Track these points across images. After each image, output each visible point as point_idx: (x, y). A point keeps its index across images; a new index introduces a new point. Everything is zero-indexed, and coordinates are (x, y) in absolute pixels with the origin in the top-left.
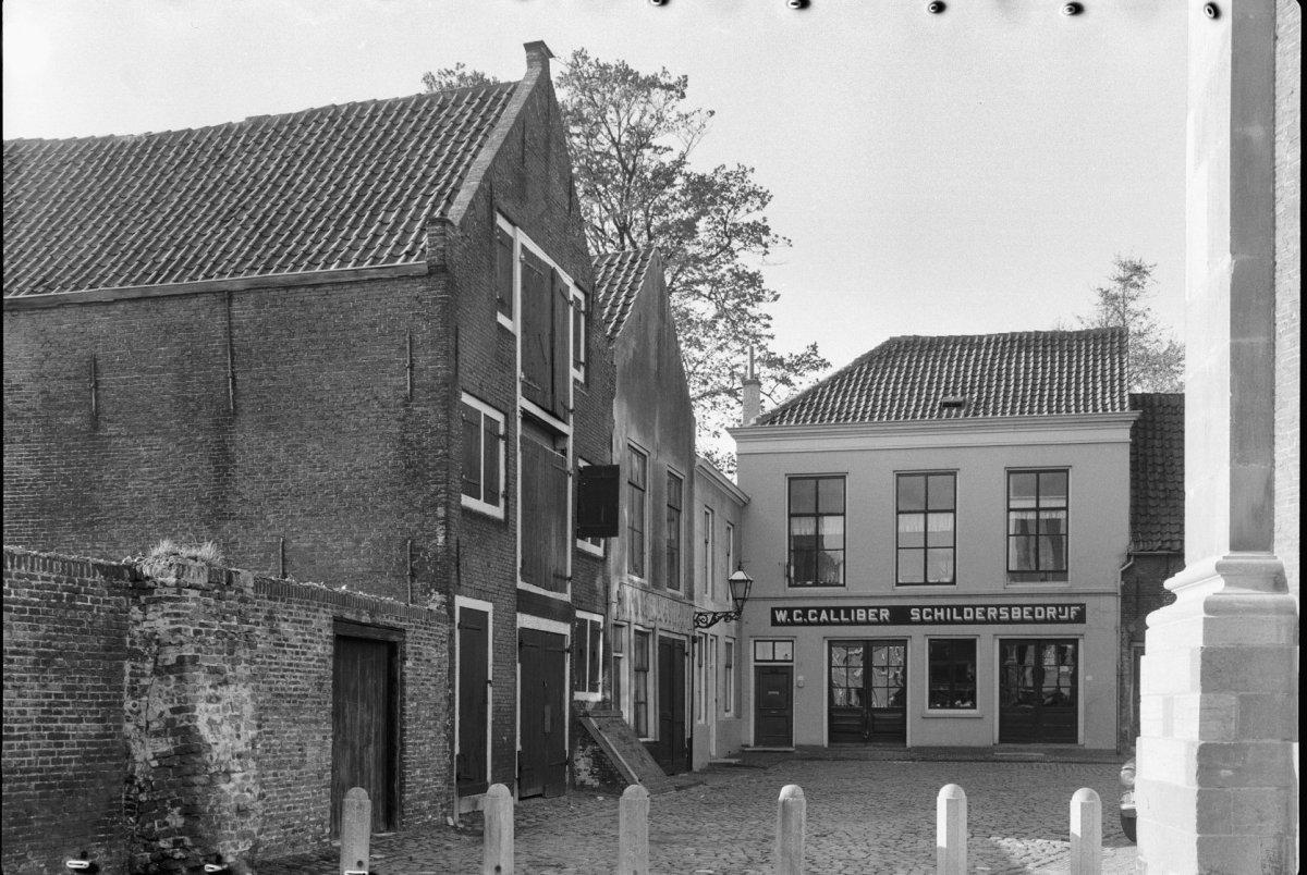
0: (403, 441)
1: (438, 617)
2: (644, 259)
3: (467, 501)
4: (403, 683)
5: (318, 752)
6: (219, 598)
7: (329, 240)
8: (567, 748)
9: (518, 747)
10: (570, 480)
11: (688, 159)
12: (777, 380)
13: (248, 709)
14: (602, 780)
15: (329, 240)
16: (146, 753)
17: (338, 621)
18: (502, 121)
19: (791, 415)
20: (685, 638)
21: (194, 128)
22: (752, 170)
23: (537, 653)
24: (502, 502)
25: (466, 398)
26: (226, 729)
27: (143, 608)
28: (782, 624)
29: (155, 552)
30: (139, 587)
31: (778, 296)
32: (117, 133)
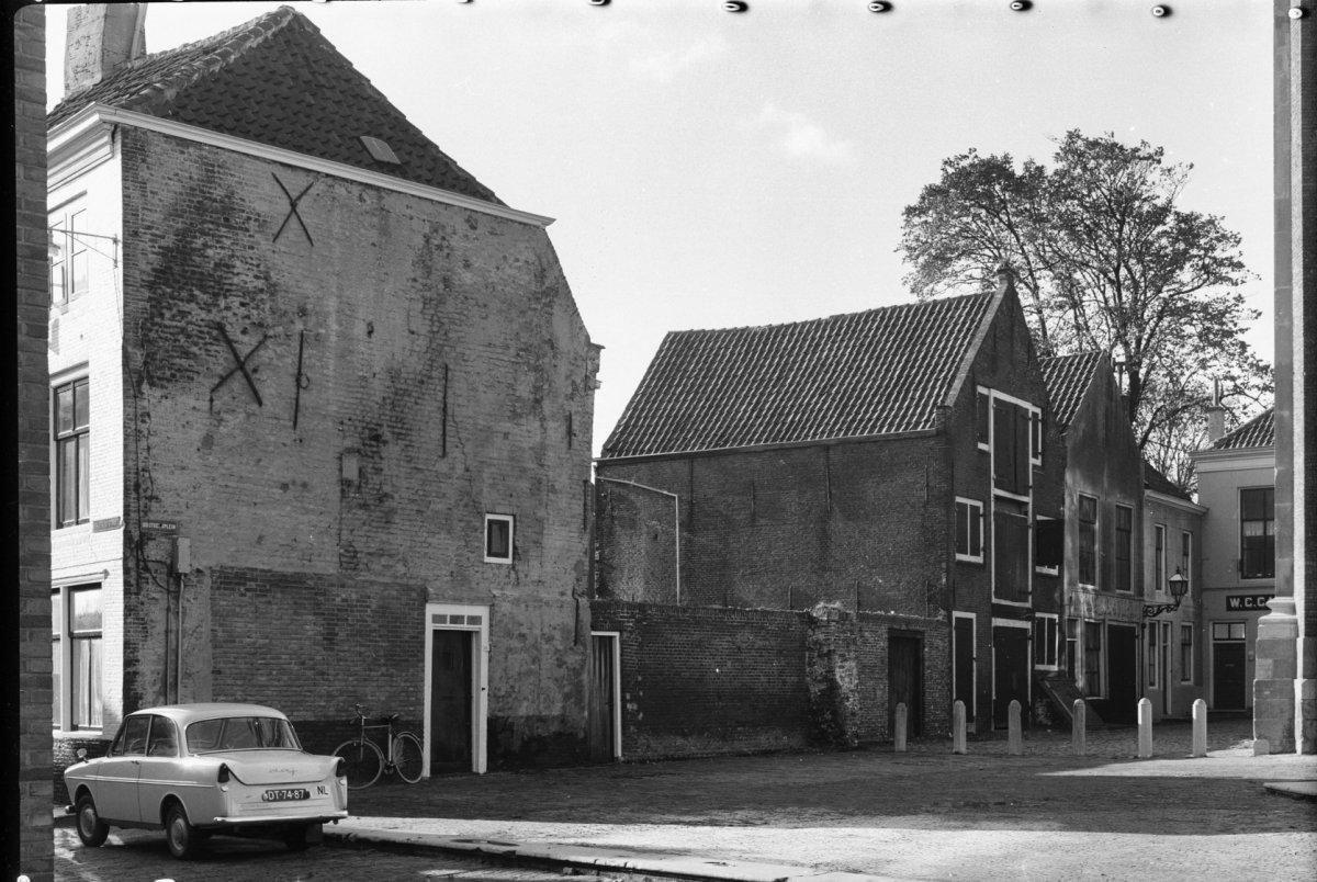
0: (923, 526)
1: (942, 623)
2: (1095, 360)
3: (960, 557)
4: (923, 660)
5: (882, 693)
6: (843, 625)
7: (883, 410)
8: (1030, 700)
9: (994, 698)
10: (1030, 531)
11: (1174, 204)
12: (1259, 389)
13: (855, 671)
14: (1053, 721)
15: (883, 410)
16: (815, 689)
17: (890, 630)
18: (982, 328)
19: (1244, 438)
20: (1134, 625)
21: (797, 322)
22: (1223, 218)
23: (1010, 643)
24: (982, 553)
25: (959, 499)
26: (847, 680)
27: (813, 630)
28: (1235, 609)
29: (818, 606)
30: (812, 622)
31: (1260, 314)
32: (751, 325)
